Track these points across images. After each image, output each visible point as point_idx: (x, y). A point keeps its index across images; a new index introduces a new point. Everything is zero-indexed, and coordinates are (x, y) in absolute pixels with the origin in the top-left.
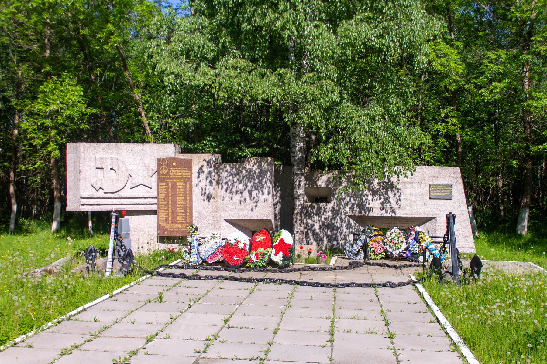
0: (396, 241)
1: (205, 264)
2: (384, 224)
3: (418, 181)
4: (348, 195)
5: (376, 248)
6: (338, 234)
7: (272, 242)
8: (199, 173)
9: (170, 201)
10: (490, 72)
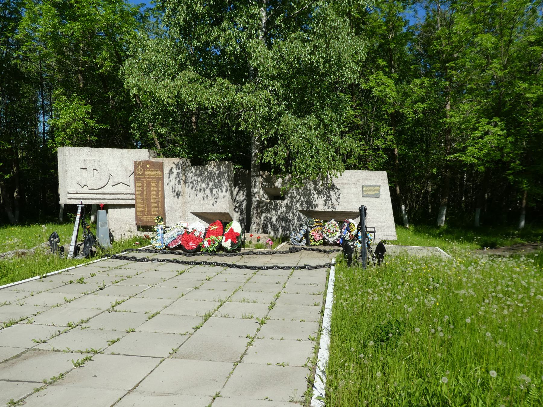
0: (331, 231)
1: (168, 249)
2: (326, 216)
3: (354, 182)
4: (299, 194)
5: (315, 236)
6: (291, 225)
7: (224, 231)
8: (169, 173)
9: (145, 197)
10: (415, 95)
